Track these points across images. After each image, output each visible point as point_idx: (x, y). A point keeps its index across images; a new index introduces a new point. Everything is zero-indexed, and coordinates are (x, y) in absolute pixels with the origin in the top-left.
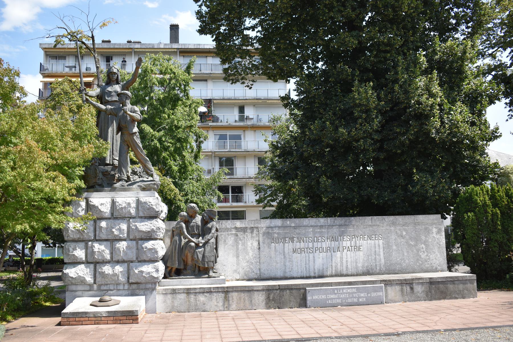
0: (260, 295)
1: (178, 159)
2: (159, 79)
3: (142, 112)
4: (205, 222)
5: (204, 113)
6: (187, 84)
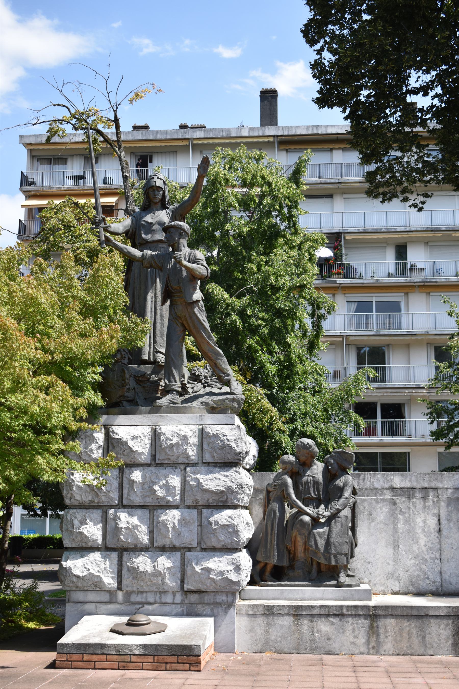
0: (442, 626)
1: (277, 350)
2: (239, 196)
3: (208, 260)
4: (331, 475)
5: (327, 260)
6: (294, 205)
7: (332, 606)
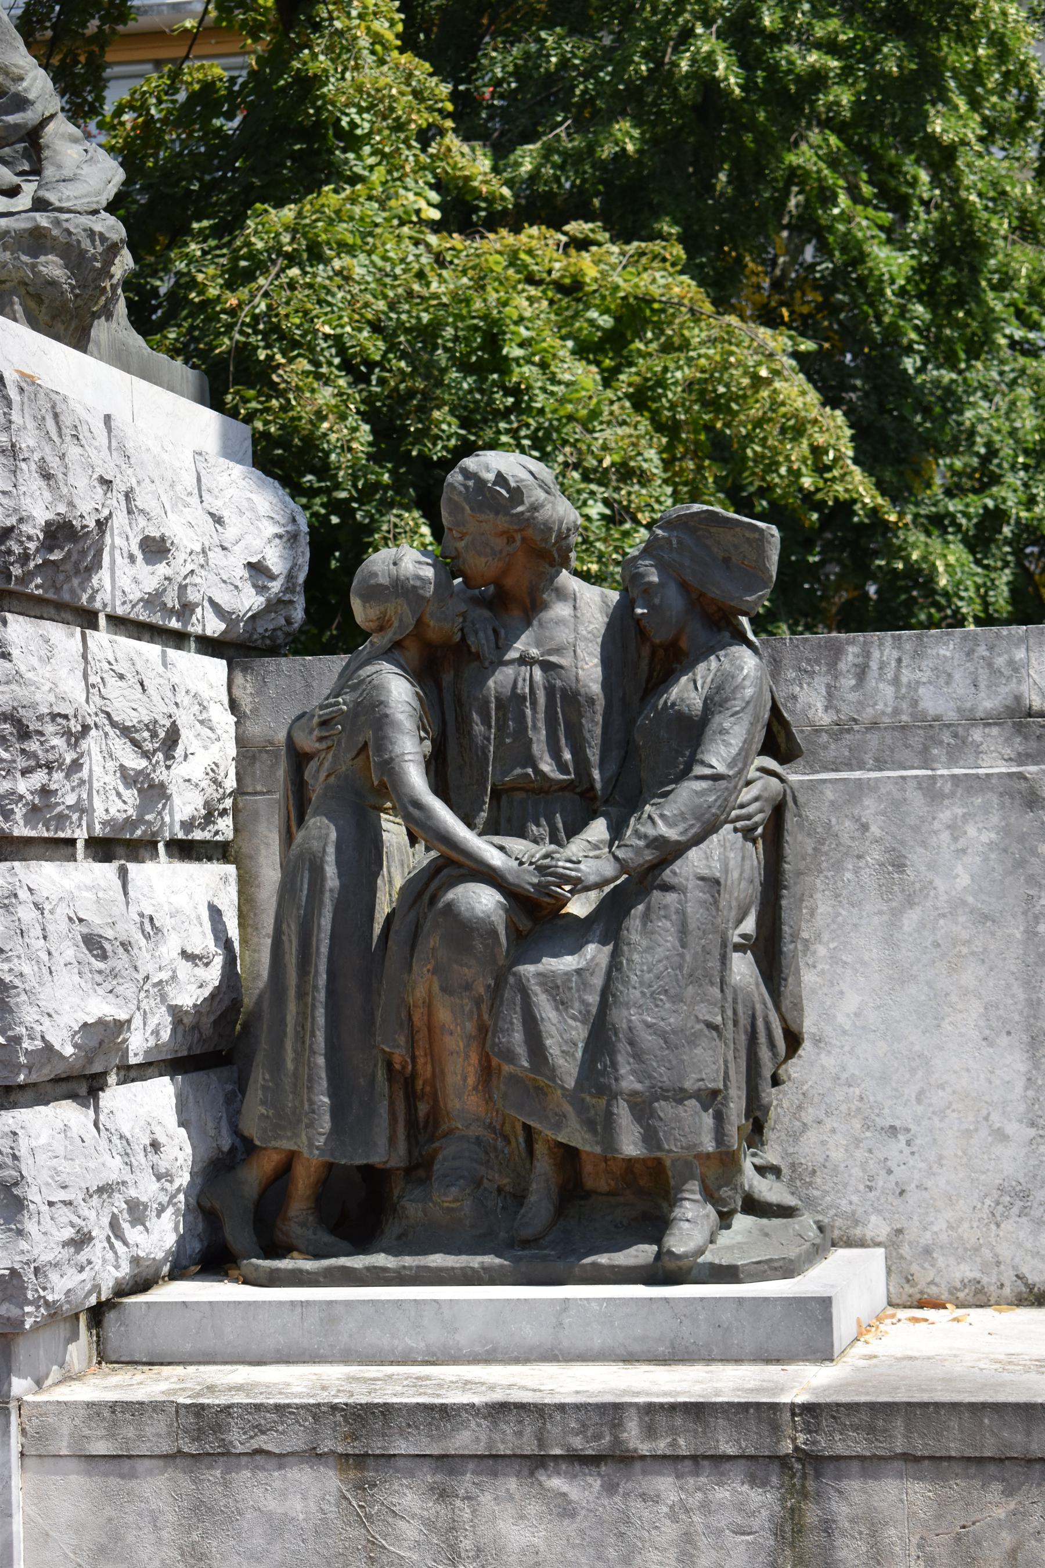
4: (646, 655)
7: (562, 1407)
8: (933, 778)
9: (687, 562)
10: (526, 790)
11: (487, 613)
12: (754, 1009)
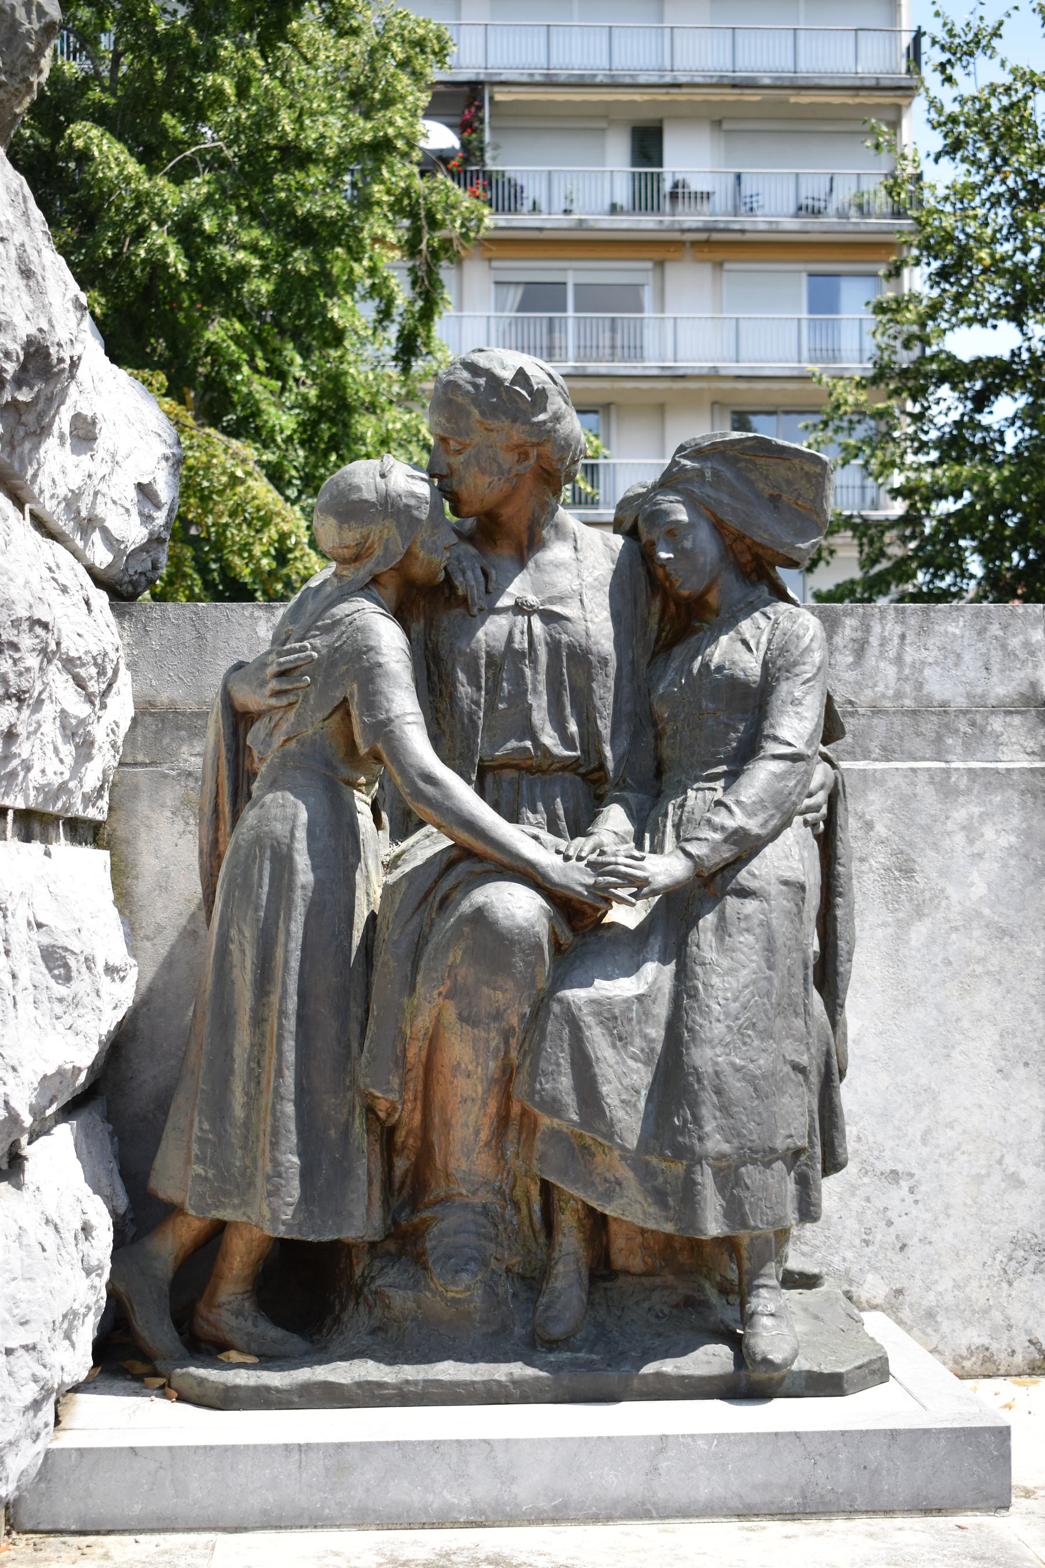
4: (666, 611)
8: (947, 771)
9: (726, 499)
10: (517, 767)
11: (473, 551)
12: (828, 1044)
